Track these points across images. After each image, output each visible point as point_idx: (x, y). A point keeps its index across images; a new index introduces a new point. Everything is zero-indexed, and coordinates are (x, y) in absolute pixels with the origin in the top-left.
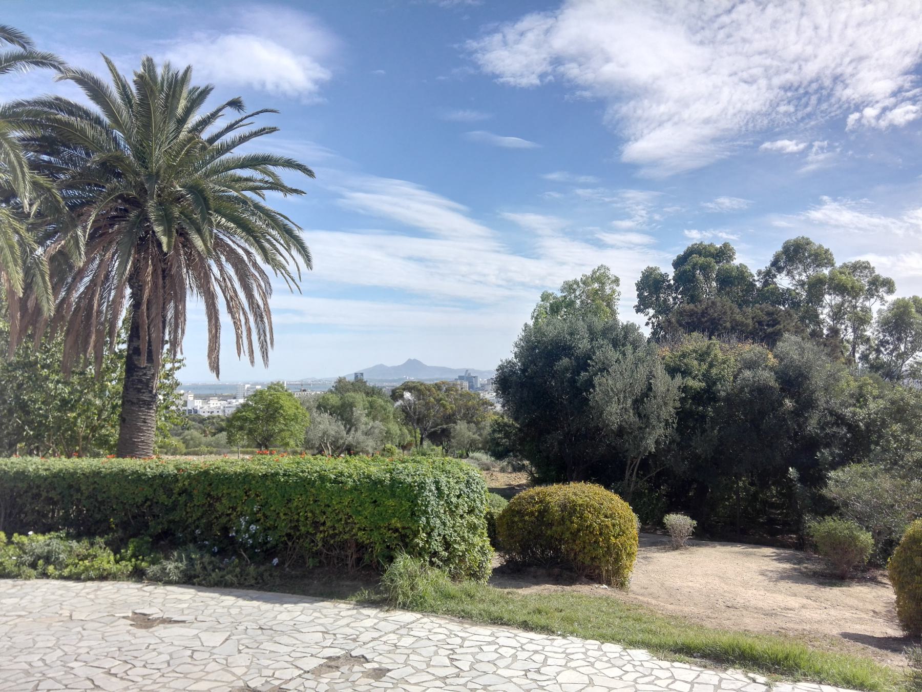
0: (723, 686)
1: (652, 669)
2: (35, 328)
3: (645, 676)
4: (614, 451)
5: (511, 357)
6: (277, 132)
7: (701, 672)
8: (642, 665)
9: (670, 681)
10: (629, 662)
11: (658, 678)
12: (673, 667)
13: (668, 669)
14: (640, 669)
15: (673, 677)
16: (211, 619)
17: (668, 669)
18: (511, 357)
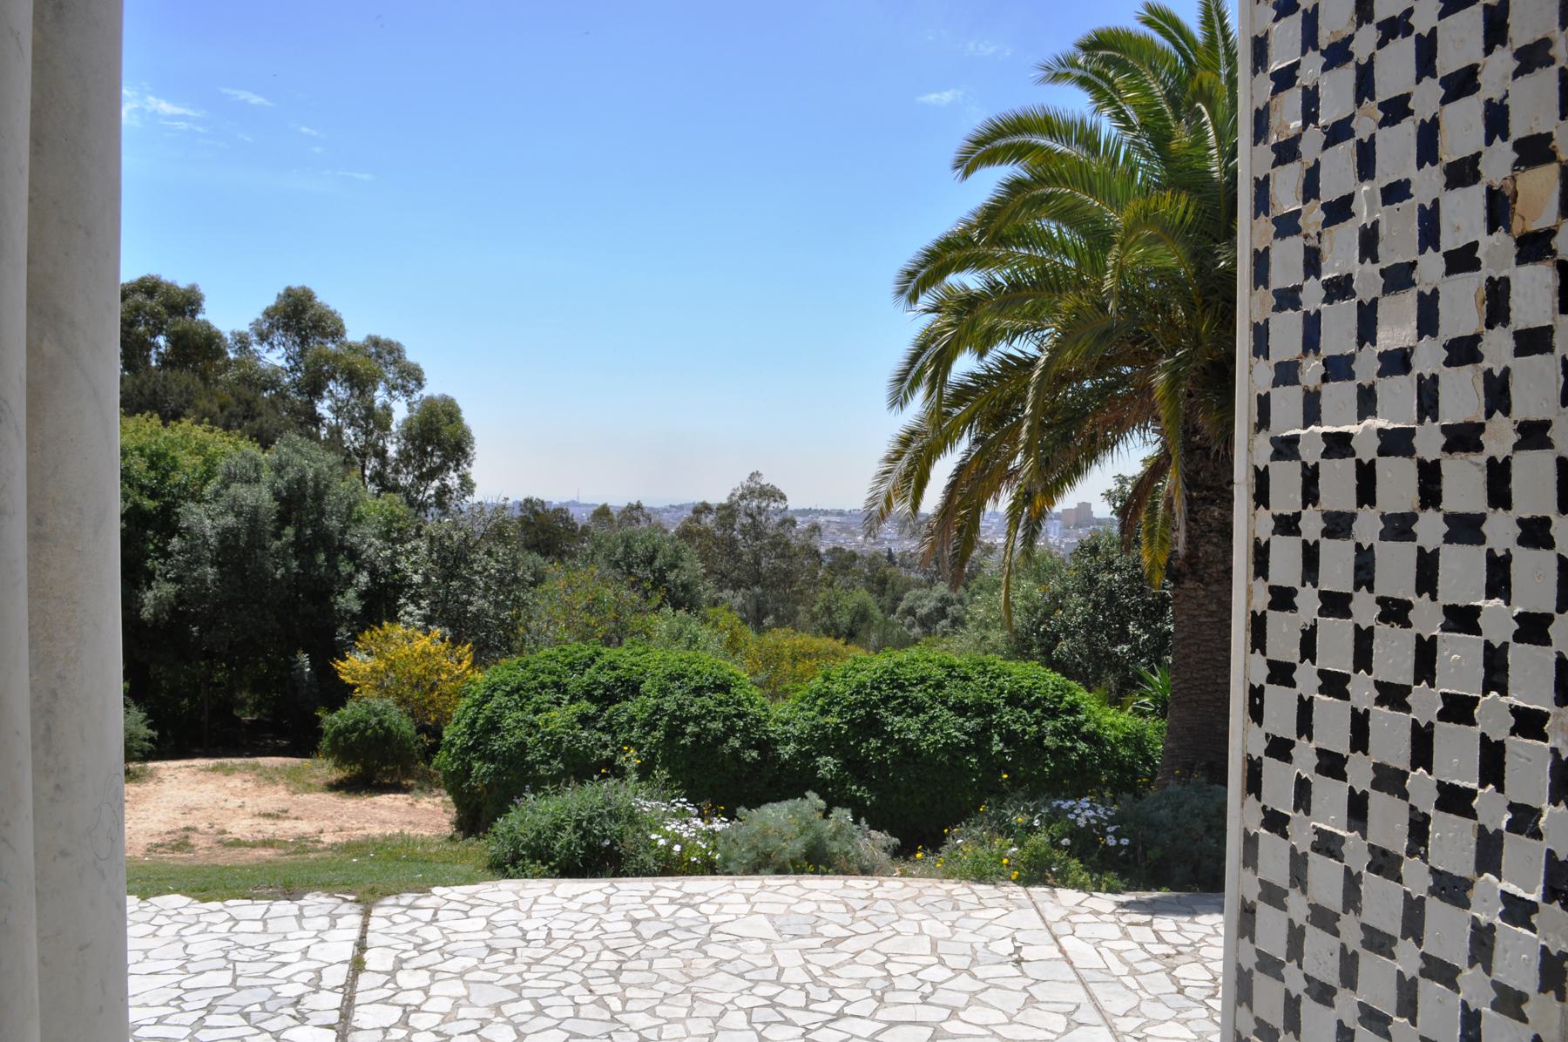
0: (306, 913)
1: (198, 915)
2: (1426, 847)
3: (191, 925)
4: (349, 601)
5: (318, 300)
6: (1413, 72)
7: (270, 904)
8: (179, 913)
9: (231, 923)
10: (157, 913)
11: (210, 924)
12: (227, 906)
13: (221, 911)
14: (179, 918)
15: (232, 918)
16: (584, 916)
17: (221, 911)
18: (318, 300)
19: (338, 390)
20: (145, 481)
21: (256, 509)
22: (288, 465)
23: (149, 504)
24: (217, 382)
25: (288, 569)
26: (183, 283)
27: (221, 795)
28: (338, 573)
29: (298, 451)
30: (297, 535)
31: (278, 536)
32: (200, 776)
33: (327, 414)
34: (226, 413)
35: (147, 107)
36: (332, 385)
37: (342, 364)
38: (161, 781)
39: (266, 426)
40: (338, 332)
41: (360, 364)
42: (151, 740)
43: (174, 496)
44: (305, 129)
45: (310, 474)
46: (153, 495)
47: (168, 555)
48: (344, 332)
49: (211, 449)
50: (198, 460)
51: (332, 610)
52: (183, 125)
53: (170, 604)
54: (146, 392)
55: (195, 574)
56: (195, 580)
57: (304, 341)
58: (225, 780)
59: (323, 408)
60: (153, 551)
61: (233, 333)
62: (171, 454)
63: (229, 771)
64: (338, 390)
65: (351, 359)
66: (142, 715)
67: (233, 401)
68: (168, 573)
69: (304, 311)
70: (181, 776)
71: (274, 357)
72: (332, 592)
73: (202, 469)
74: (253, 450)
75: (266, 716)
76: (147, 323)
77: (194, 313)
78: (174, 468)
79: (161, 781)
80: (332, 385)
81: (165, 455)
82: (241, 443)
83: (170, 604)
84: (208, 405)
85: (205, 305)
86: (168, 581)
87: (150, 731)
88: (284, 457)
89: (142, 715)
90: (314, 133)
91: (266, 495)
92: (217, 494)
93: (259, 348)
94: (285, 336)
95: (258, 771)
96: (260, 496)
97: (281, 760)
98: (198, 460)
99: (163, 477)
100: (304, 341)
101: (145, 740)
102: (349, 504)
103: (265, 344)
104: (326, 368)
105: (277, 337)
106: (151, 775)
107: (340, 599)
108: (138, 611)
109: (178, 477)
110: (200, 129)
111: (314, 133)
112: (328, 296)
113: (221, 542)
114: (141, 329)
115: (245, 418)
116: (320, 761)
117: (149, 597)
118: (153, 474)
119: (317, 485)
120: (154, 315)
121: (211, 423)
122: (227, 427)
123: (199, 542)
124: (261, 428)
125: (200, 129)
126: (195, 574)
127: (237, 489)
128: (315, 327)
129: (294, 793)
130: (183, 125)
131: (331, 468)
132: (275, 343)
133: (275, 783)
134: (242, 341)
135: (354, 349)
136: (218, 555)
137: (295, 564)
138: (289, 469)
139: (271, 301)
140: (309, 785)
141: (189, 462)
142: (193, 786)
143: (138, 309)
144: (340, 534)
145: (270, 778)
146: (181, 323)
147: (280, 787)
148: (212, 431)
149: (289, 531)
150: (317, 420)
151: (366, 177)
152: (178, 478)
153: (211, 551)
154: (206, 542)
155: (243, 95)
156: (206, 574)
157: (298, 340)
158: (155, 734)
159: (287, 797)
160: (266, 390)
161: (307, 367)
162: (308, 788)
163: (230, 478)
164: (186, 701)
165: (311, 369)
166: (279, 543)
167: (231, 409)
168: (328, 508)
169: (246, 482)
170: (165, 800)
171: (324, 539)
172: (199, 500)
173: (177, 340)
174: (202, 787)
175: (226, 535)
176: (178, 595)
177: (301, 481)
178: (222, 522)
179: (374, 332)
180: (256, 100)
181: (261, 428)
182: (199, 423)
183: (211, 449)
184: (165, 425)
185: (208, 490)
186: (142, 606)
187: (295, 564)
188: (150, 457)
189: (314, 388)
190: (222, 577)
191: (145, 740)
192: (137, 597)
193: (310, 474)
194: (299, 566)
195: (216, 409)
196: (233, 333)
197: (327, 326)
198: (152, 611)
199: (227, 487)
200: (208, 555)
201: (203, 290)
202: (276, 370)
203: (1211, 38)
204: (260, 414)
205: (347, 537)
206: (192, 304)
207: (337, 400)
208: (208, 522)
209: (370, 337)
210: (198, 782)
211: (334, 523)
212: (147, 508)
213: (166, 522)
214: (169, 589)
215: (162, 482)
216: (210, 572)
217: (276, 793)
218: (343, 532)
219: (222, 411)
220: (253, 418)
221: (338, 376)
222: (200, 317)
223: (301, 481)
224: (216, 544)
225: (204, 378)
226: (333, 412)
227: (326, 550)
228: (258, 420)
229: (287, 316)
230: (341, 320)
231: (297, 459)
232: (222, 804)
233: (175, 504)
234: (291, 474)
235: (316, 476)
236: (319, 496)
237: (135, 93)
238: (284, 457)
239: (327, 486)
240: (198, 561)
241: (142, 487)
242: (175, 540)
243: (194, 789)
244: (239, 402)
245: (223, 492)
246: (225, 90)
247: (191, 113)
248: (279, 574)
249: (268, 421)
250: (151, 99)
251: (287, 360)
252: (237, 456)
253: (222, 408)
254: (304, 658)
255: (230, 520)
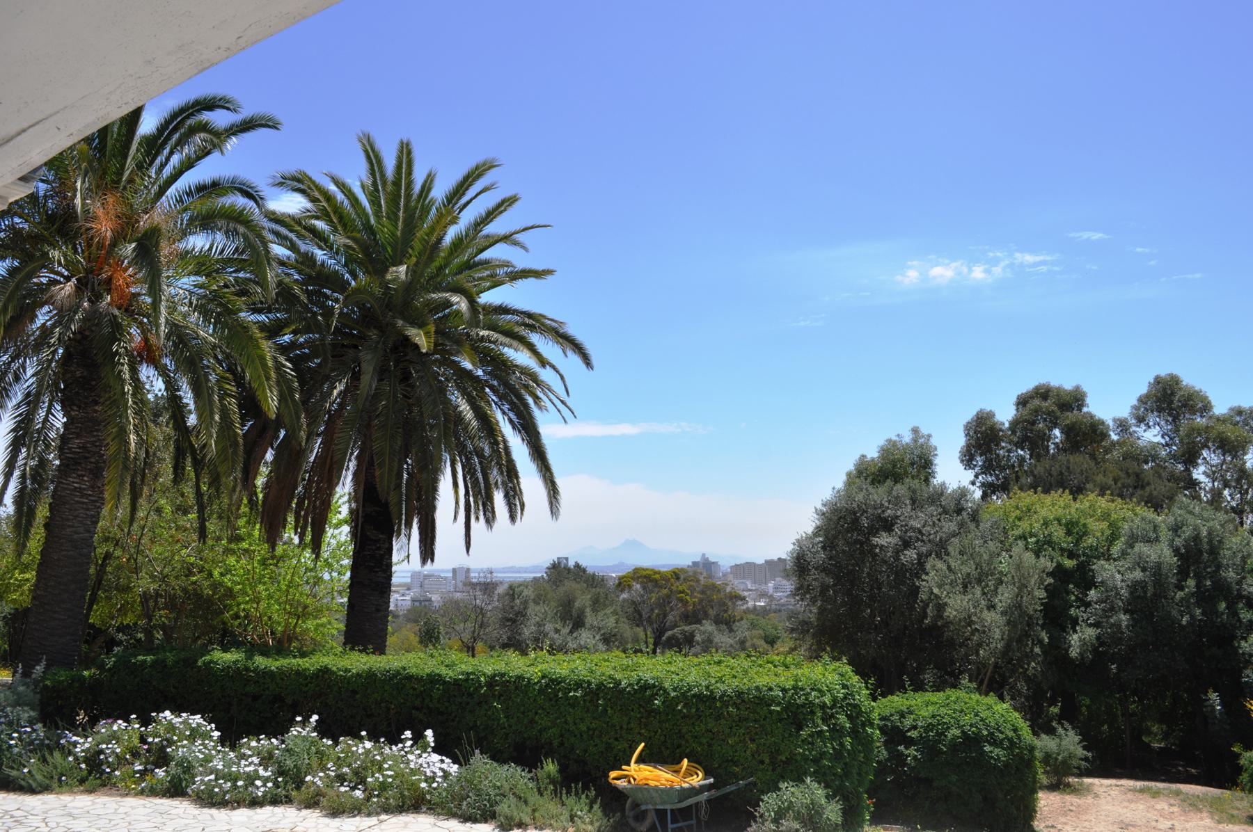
18: (1184, 383)
19: (1211, 457)
20: (1064, 545)
21: (1159, 565)
22: (1183, 525)
23: (1069, 563)
24: (1104, 461)
25: (1192, 617)
26: (1068, 386)
27: (1152, 815)
28: (1239, 620)
29: (1190, 513)
30: (1197, 586)
31: (1181, 588)
32: (1130, 796)
33: (1202, 478)
34: (1119, 484)
35: (1016, 261)
36: (1205, 453)
37: (1213, 434)
38: (1097, 796)
39: (1155, 493)
40: (1206, 407)
41: (1230, 433)
42: (1086, 759)
43: (1088, 556)
44: (1139, 250)
45: (1204, 533)
46: (1071, 555)
47: (1088, 605)
48: (1211, 407)
49: (1114, 516)
50: (1105, 525)
51: (1236, 653)
52: (1044, 268)
53: (1093, 645)
54: (1054, 473)
55: (1112, 621)
56: (1113, 625)
57: (1176, 419)
58: (1152, 802)
59: (1199, 474)
60: (1075, 601)
61: (1114, 420)
62: (1082, 521)
63: (1156, 794)
64: (1211, 457)
65: (1221, 428)
66: (1078, 738)
67: (1122, 475)
68: (1088, 619)
69: (1173, 394)
70: (1112, 793)
71: (1151, 435)
72: (1234, 637)
73: (1108, 532)
74: (1150, 514)
75: (1174, 744)
76: (1045, 420)
77: (1080, 408)
78: (1085, 534)
79: (1097, 796)
80: (1205, 453)
81: (1077, 523)
82: (1138, 509)
83: (1093, 645)
84: (1104, 480)
85: (1088, 400)
86: (1090, 625)
87: (1085, 752)
88: (1179, 519)
89: (1078, 738)
90: (1147, 250)
91: (1167, 552)
92: (1124, 554)
93: (1137, 429)
94: (1159, 417)
95: (1181, 797)
96: (1162, 553)
97: (1199, 788)
98: (1105, 525)
99: (1077, 541)
100: (1176, 419)
101: (1082, 759)
102: (1243, 557)
103: (1142, 425)
104: (1198, 439)
105: (1152, 418)
106: (1088, 790)
107: (1243, 643)
108: (1067, 650)
109: (1090, 541)
110: (1057, 269)
111: (1147, 250)
112: (1192, 379)
113: (1131, 593)
114: (1041, 426)
115: (1135, 487)
116: (1239, 794)
117: (1075, 639)
118: (1070, 539)
119: (1210, 542)
120: (1049, 413)
121: (1112, 494)
122: (1121, 496)
123: (1113, 593)
124: (1151, 494)
125: (1057, 269)
126: (1112, 621)
127: (1141, 548)
128: (1185, 405)
129: (1219, 822)
130: (1044, 268)
131: (1222, 526)
132: (1151, 424)
133: (1200, 811)
134: (1122, 425)
135: (1221, 420)
136: (1129, 604)
137: (1198, 612)
138: (1184, 528)
139: (1144, 390)
140: (1233, 816)
141: (1098, 527)
142: (1127, 804)
143: (1036, 411)
144: (1237, 584)
145: (1193, 805)
146: (1071, 417)
147: (1205, 814)
148: (1113, 501)
149: (1191, 583)
150: (1193, 484)
151: (1198, 276)
152: (1090, 541)
153: (1122, 600)
154: (1118, 593)
155: (1086, 235)
156: (1121, 621)
157: (1170, 419)
158: (1090, 754)
159: (1213, 825)
160: (1147, 463)
161: (1181, 441)
162: (1232, 819)
163: (1133, 539)
164: (1106, 727)
165: (1186, 441)
166: (1182, 593)
167: (1123, 481)
168: (1225, 562)
169: (1148, 542)
170: (1103, 813)
171: (1222, 589)
172: (1109, 558)
173: (1069, 431)
174: (1133, 806)
175: (1135, 586)
176: (1098, 638)
177: (1197, 538)
178: (1131, 576)
179: (1236, 404)
180: (1097, 236)
181: (1151, 494)
182: (1103, 495)
183: (1114, 516)
184: (1075, 499)
185: (1115, 550)
186: (1069, 647)
187: (1198, 612)
188: (1067, 525)
189: (1190, 457)
190: (1135, 623)
191: (1082, 759)
192: (1065, 638)
193: (1204, 533)
194: (1202, 614)
195: (1111, 482)
196: (1114, 420)
197: (1193, 403)
198: (1078, 651)
199: (1132, 547)
200: (1120, 604)
201: (1085, 388)
202: (1154, 446)
203: (397, 183)
204: (1149, 484)
205: (1244, 586)
206: (1078, 400)
207: (1212, 466)
208: (1118, 577)
209: (1232, 409)
210: (1130, 801)
211: (1231, 575)
212: (1068, 566)
213: (1083, 577)
214: (1090, 633)
215: (1077, 543)
216: (1124, 618)
217: (1202, 819)
218: (1239, 583)
219: (1115, 484)
220: (1143, 487)
221: (1210, 444)
222: (1085, 410)
223: (1197, 538)
224: (1126, 595)
225: (1093, 457)
226: (1208, 476)
227: (1226, 599)
228: (1148, 489)
229: (1158, 400)
230: (1207, 397)
231: (1191, 520)
232: (1154, 823)
233: (1088, 563)
234: (1187, 532)
235: (1210, 534)
236: (1214, 551)
237: (1006, 253)
238: (1179, 519)
239: (1220, 542)
240: (1112, 609)
241: (1062, 549)
242: (1092, 592)
243: (1127, 808)
244: (1128, 474)
245: (1129, 551)
246: (1072, 235)
247: (1049, 258)
248: (1185, 620)
249: (1159, 488)
250: (1018, 255)
251: (1163, 437)
252: (1138, 520)
253: (1116, 480)
254: (1214, 697)
255: (1138, 575)
